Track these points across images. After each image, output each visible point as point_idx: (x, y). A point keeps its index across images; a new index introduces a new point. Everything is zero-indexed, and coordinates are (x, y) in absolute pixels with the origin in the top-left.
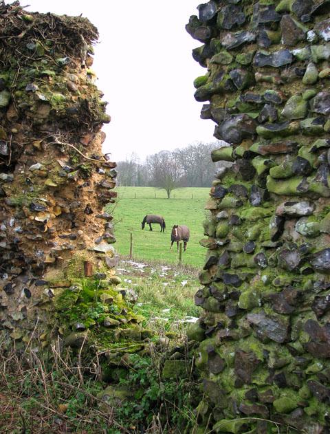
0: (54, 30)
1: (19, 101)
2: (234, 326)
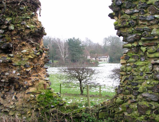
0: (29, 3)
1: (18, 28)
2: (136, 98)
